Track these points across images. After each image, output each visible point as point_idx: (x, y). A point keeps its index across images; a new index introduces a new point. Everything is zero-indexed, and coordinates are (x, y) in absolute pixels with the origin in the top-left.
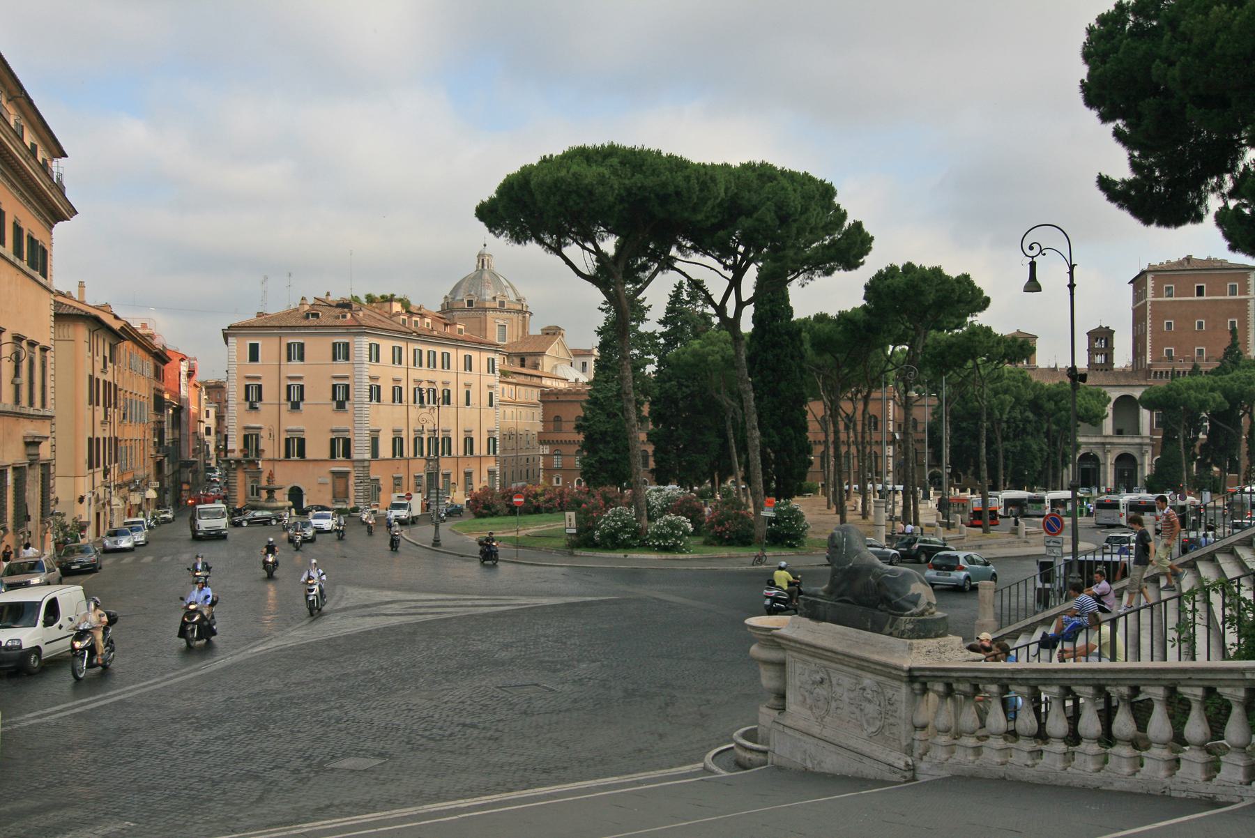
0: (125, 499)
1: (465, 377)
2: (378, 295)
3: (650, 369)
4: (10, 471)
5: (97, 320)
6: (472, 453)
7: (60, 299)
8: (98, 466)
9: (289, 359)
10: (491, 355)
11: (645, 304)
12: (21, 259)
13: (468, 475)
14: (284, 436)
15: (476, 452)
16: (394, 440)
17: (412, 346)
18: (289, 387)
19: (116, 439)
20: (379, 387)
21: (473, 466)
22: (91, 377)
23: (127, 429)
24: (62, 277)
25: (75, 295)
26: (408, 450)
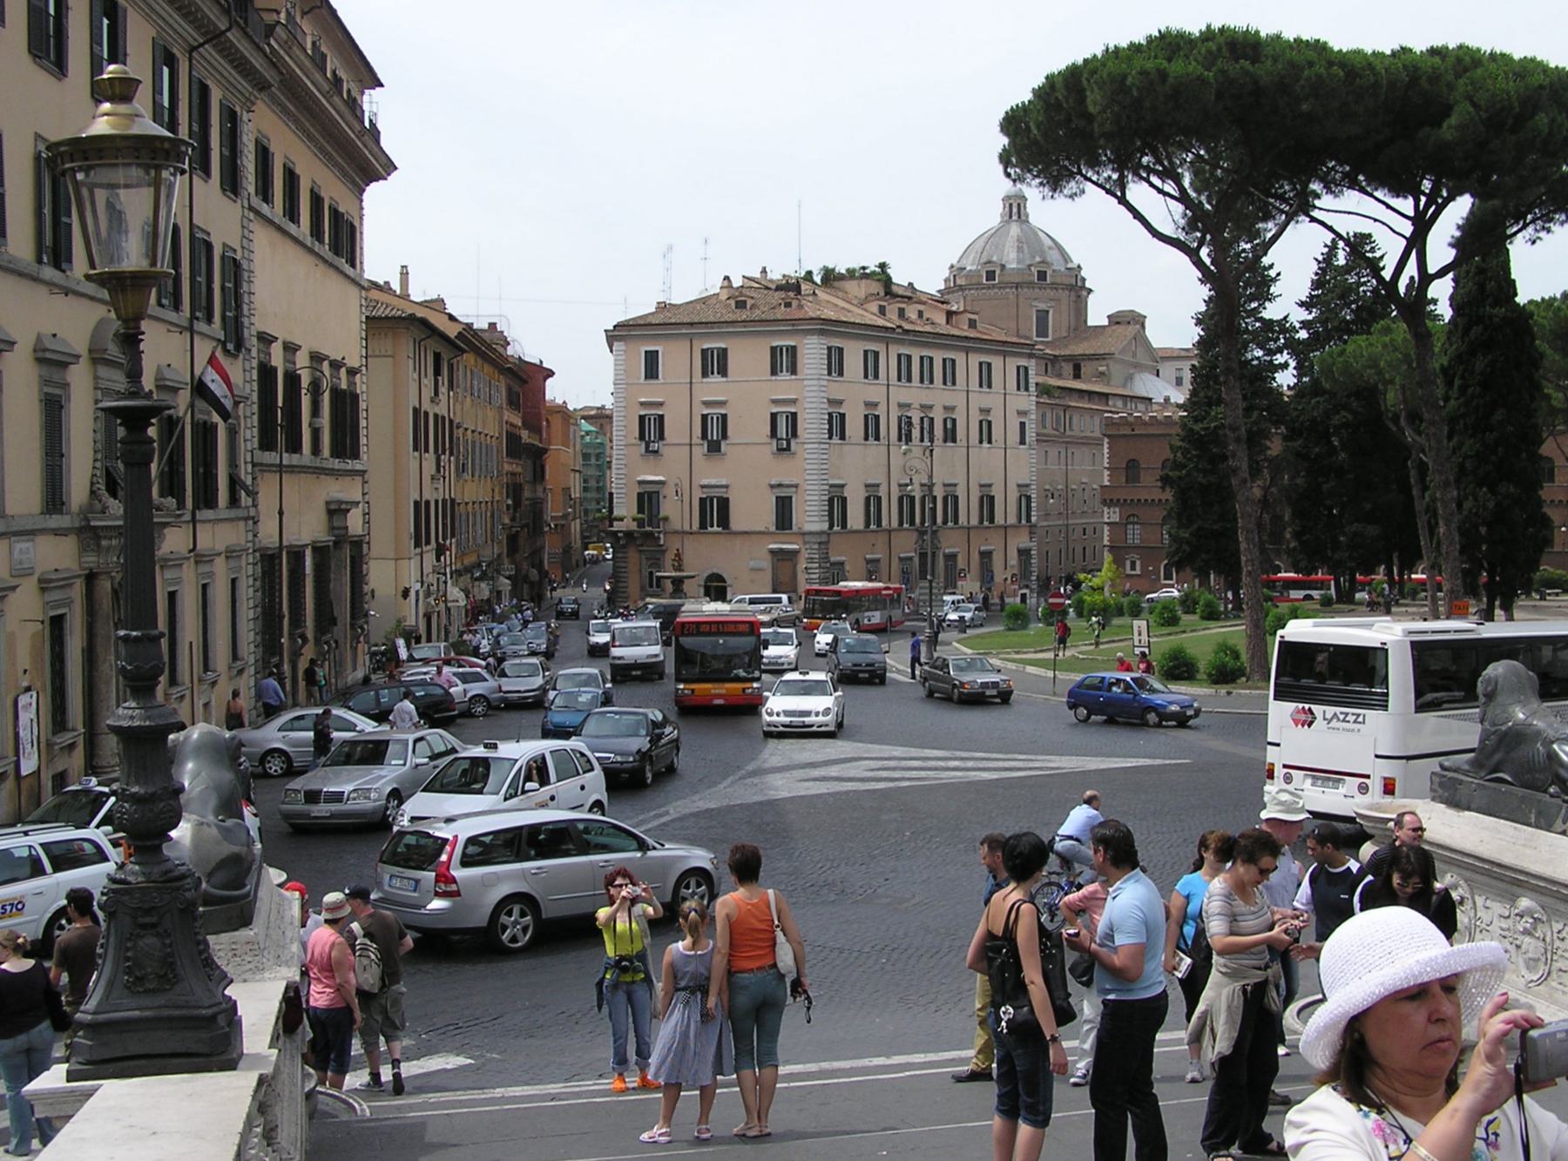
0: (467, 592)
1: (980, 399)
2: (841, 269)
3: (1285, 379)
4: (308, 553)
5: (424, 323)
6: (992, 520)
7: (375, 294)
8: (428, 542)
9: (705, 374)
10: (1023, 362)
11: (1272, 273)
12: (321, 241)
13: (986, 556)
14: (698, 494)
15: (999, 519)
16: (868, 499)
17: (895, 350)
18: (704, 417)
19: (453, 501)
20: (843, 416)
21: (993, 544)
22: (416, 411)
23: (468, 486)
24: (377, 263)
25: (396, 286)
26: (890, 516)
